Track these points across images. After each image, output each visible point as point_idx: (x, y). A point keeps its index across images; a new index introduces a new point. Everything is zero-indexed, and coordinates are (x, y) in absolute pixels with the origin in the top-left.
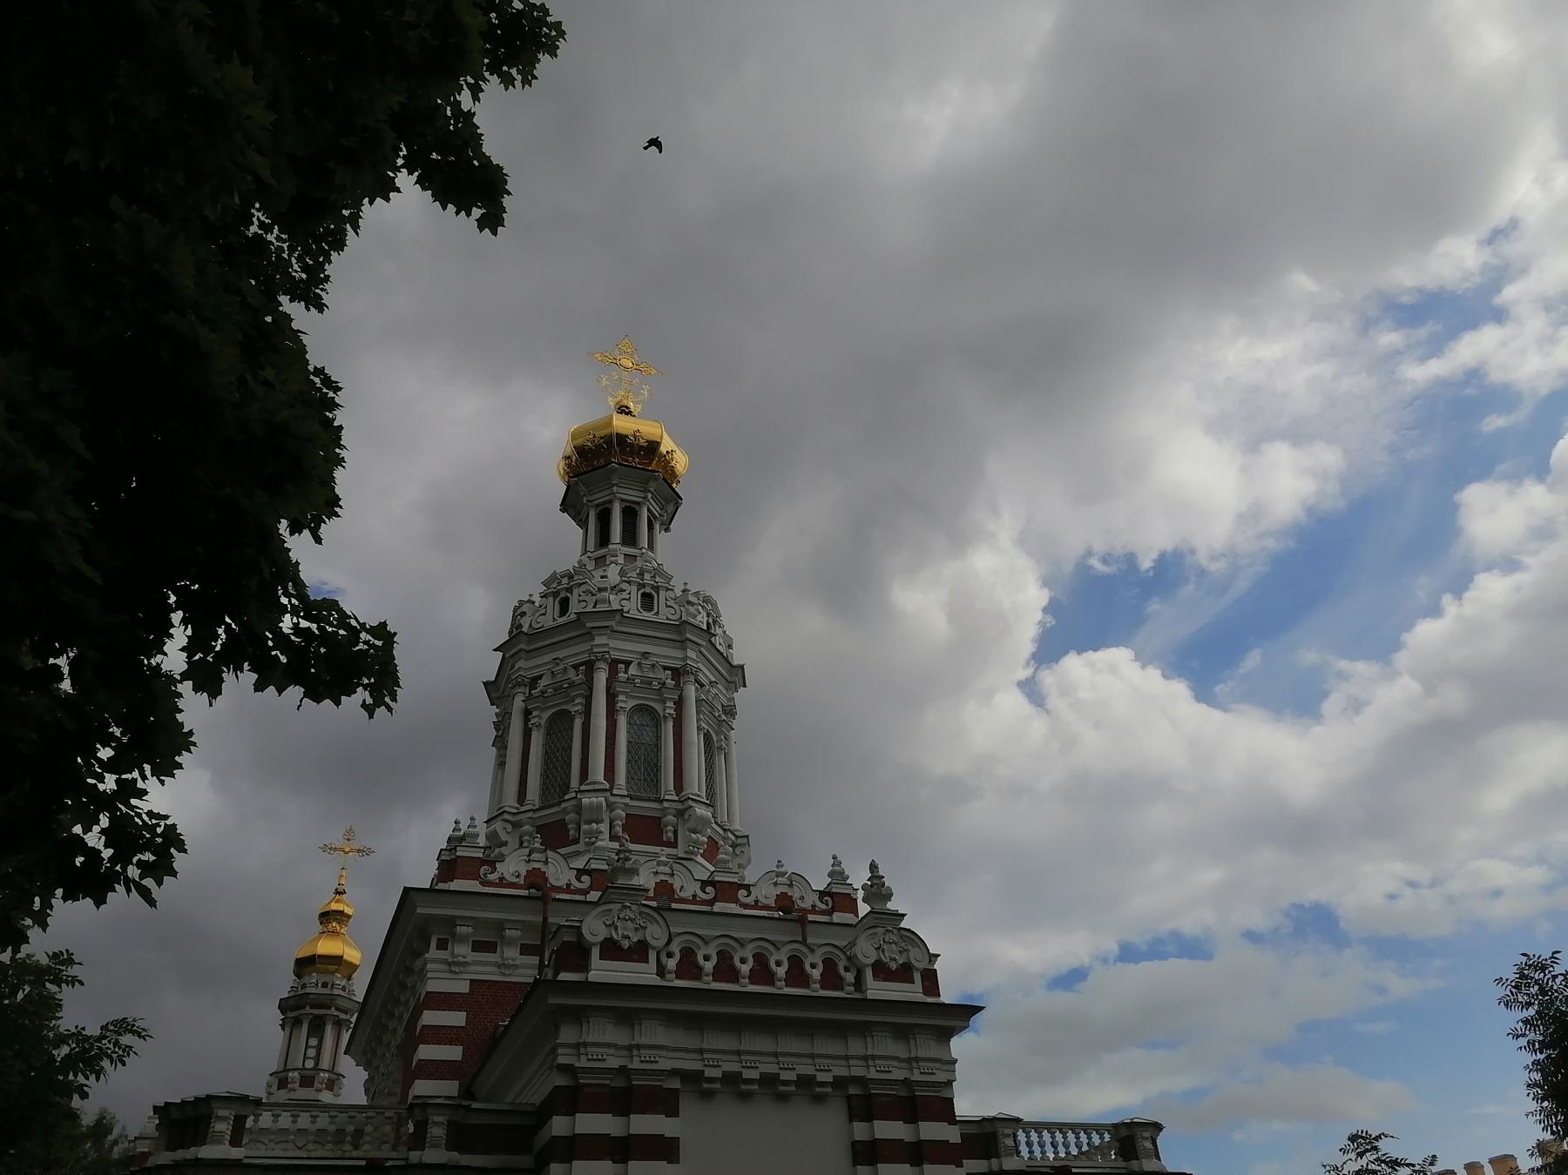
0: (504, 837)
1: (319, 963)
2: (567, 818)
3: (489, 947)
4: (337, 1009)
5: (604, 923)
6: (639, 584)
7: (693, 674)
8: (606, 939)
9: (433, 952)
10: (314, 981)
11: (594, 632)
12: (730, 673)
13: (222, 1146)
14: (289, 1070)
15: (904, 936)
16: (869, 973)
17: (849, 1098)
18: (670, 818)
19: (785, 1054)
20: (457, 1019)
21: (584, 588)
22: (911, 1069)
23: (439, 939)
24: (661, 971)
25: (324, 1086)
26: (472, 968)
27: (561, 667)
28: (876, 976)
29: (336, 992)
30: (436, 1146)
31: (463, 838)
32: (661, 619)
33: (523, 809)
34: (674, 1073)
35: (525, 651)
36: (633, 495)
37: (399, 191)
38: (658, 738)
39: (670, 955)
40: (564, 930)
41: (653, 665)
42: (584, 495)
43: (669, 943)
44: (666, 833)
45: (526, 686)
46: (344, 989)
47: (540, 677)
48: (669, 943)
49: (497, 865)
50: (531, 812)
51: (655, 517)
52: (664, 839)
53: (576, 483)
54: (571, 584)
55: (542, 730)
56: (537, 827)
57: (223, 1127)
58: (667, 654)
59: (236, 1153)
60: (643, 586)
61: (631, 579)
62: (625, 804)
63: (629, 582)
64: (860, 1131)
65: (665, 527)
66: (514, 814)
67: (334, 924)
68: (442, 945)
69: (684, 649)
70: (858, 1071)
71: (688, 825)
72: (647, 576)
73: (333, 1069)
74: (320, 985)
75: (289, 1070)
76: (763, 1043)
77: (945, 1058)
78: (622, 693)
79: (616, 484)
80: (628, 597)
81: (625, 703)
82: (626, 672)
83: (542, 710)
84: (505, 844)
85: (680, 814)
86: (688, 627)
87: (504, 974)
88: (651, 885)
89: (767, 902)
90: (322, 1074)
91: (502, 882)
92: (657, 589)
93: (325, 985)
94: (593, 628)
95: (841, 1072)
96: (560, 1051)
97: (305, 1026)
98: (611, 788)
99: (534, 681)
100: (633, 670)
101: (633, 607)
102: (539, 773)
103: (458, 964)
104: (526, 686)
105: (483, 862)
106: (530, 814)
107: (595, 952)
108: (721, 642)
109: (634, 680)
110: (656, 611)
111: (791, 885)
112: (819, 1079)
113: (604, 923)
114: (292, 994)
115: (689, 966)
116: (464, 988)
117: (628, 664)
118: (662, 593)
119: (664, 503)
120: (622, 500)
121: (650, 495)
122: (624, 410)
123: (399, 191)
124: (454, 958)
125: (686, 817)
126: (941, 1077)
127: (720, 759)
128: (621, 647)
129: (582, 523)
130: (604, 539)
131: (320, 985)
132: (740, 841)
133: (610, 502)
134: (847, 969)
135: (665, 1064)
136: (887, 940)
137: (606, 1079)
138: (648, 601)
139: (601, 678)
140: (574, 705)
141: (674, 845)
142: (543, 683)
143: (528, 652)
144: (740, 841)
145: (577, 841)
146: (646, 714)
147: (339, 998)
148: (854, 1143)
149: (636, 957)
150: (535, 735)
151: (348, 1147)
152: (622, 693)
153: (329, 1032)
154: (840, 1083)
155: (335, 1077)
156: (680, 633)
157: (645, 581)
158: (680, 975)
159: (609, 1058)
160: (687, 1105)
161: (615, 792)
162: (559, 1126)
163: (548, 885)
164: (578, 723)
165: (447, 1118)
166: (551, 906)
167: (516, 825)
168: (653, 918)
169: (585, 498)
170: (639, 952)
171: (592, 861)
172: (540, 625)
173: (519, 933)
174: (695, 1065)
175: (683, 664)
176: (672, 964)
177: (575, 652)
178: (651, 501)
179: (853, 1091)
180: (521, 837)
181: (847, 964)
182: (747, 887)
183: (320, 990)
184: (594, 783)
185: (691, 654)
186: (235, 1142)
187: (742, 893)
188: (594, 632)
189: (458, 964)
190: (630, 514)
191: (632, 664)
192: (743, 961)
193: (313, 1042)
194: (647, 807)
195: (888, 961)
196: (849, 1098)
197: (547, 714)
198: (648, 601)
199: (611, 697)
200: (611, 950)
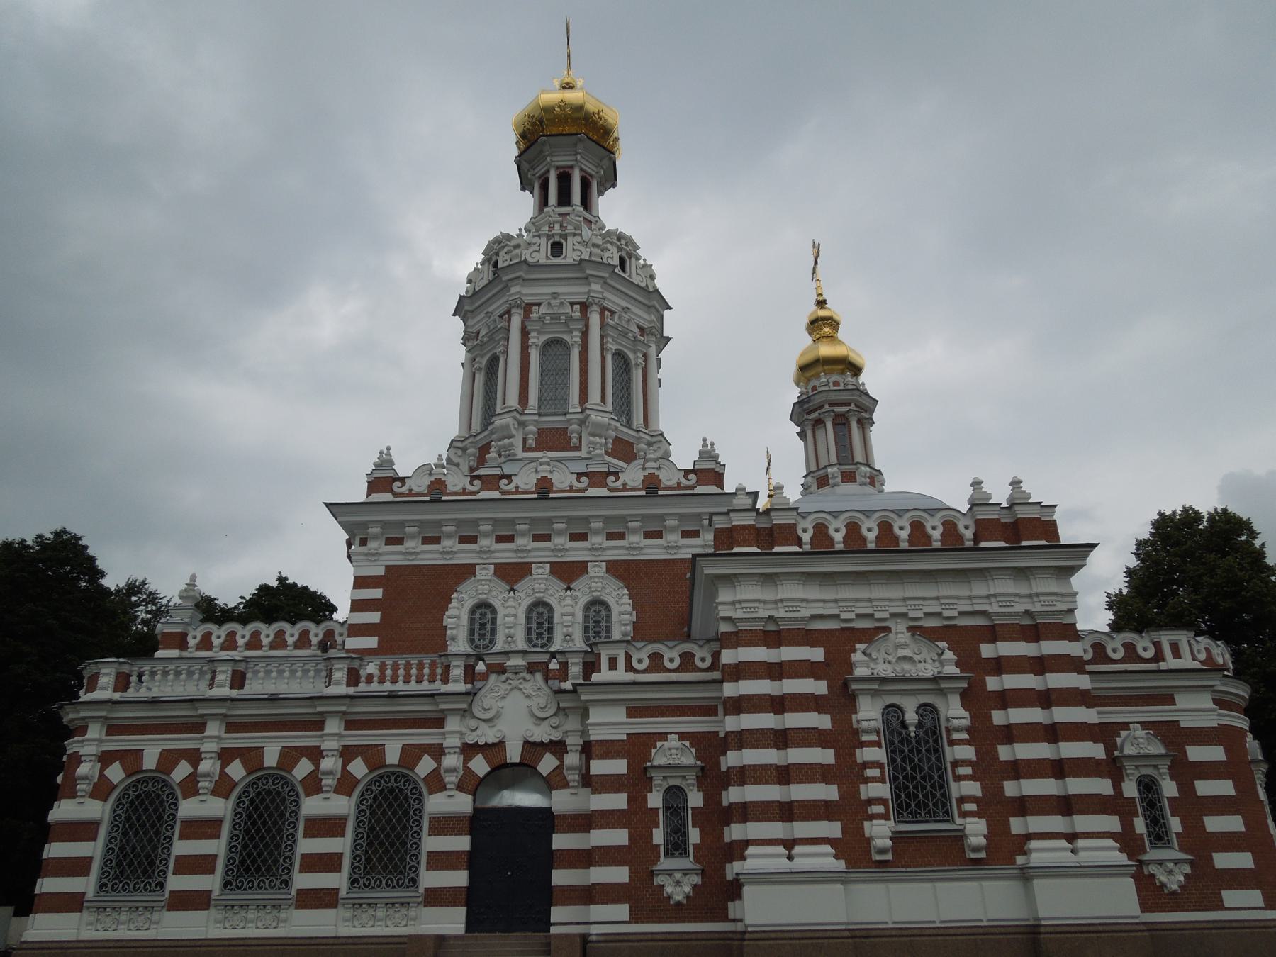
6: (548, 235)
7: (596, 304)
11: (591, 279)
12: (649, 299)
18: (643, 446)
19: (1001, 595)
22: (1033, 603)
26: (532, 554)
30: (456, 681)
32: (569, 261)
35: (469, 311)
36: (563, 161)
42: (529, 170)
49: (513, 478)
55: (483, 372)
58: (576, 292)
60: (553, 236)
66: (462, 441)
76: (894, 592)
77: (1070, 591)
78: (534, 330)
79: (580, 153)
80: (537, 249)
81: (536, 339)
85: (582, 423)
88: (639, 483)
89: (527, 487)
91: (410, 494)
94: (509, 280)
101: (542, 256)
102: (480, 407)
103: (560, 550)
105: (609, 474)
108: (639, 271)
112: (876, 617)
116: (380, 571)
118: (570, 239)
121: (579, 157)
122: (567, 86)
126: (1062, 607)
128: (529, 293)
130: (544, 202)
132: (655, 439)
137: (1016, 619)
139: (595, 319)
141: (579, 448)
143: (472, 312)
144: (655, 439)
146: (555, 347)
151: (438, 682)
152: (534, 330)
156: (583, 271)
159: (1016, 604)
173: (527, 526)
178: (583, 161)
182: (402, 480)
185: (596, 287)
187: (398, 484)
188: (591, 279)
190: (564, 179)
199: (525, 333)
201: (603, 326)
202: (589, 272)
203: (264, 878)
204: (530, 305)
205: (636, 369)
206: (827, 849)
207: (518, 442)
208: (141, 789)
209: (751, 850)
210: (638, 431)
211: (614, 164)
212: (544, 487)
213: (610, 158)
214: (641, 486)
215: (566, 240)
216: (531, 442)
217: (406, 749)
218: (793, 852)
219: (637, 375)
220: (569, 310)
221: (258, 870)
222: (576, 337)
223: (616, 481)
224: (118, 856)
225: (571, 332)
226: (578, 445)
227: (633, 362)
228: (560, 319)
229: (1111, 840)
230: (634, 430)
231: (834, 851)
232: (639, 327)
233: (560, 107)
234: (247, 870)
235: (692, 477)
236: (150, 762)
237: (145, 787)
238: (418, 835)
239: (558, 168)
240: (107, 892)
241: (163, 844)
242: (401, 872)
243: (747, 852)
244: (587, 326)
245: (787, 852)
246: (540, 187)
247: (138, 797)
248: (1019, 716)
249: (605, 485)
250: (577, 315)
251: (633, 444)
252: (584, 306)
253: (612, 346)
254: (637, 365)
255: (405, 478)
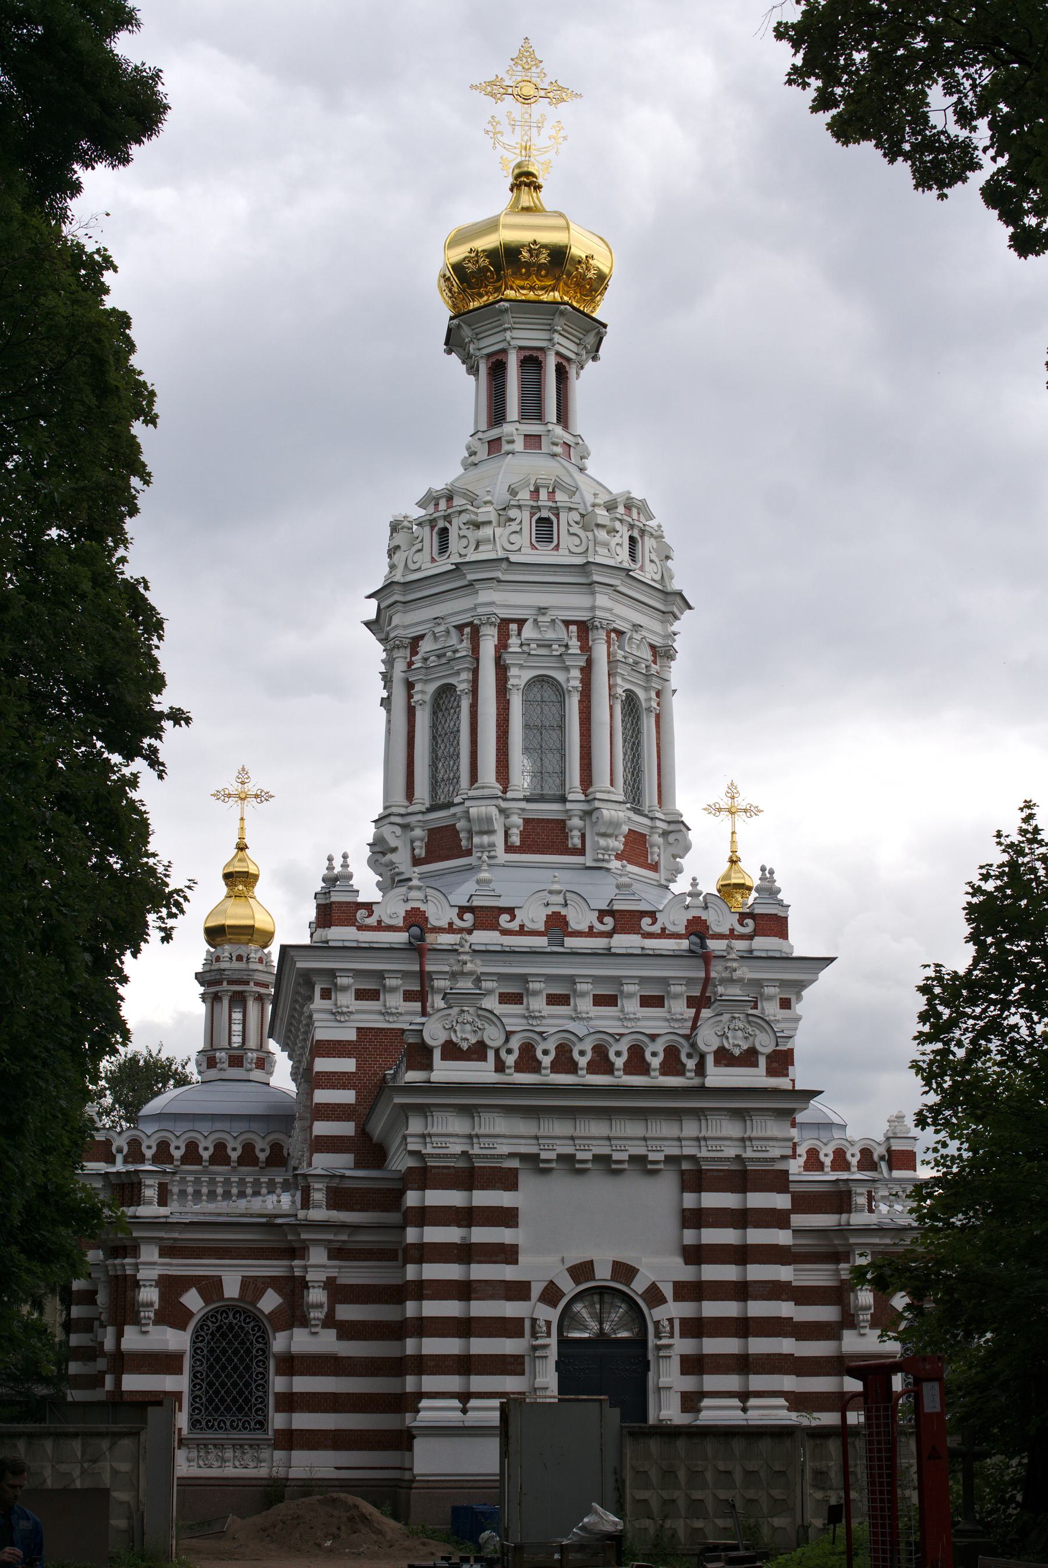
0: (393, 843)
1: (230, 934)
2: (459, 826)
3: (372, 995)
4: (257, 984)
5: (444, 1027)
6: (532, 507)
7: (603, 628)
8: (446, 1041)
9: (318, 1002)
10: (226, 954)
12: (665, 602)
13: (152, 1207)
14: (215, 1050)
15: (753, 1022)
16: (710, 1060)
17: (682, 1173)
20: (348, 1065)
21: (465, 517)
23: (322, 989)
24: (500, 1067)
25: (254, 1065)
27: (442, 628)
28: (717, 1062)
29: (252, 966)
31: (336, 879)
33: (411, 809)
34: (512, 1155)
37: (155, 427)
38: (563, 717)
39: (509, 1051)
40: (407, 1033)
41: (553, 621)
43: (507, 1040)
44: (572, 838)
45: (406, 647)
46: (261, 960)
47: (422, 637)
48: (507, 1040)
50: (420, 815)
51: (569, 360)
52: (570, 846)
53: (459, 326)
54: (449, 511)
56: (428, 830)
57: (150, 1193)
59: (163, 1211)
60: (539, 508)
61: (521, 502)
62: (523, 810)
63: (519, 507)
64: (689, 1200)
65: (593, 355)
66: (402, 815)
67: (241, 887)
68: (326, 994)
69: (593, 593)
70: (687, 1151)
71: (597, 829)
72: (543, 494)
73: (261, 1047)
74: (234, 958)
75: (215, 1050)
80: (518, 528)
81: (519, 677)
82: (519, 634)
83: (426, 681)
84: (394, 850)
86: (593, 567)
87: (389, 1022)
90: (249, 1054)
92: (556, 511)
93: (240, 958)
95: (676, 1151)
96: (409, 1140)
97: (226, 1003)
98: (505, 792)
99: (415, 642)
100: (528, 632)
103: (342, 1013)
104: (406, 647)
105: (644, 914)
106: (420, 817)
107: (437, 1054)
109: (529, 645)
110: (555, 542)
111: (706, 908)
113: (444, 1027)
114: (208, 968)
115: (528, 1061)
116: (351, 1035)
117: (521, 622)
118: (563, 516)
119: (581, 336)
120: (558, 354)
123: (155, 427)
124: (337, 1008)
125: (594, 819)
127: (648, 723)
129: (473, 370)
130: (497, 414)
131: (234, 958)
132: (672, 827)
133: (504, 351)
134: (689, 1056)
135: (504, 1149)
136: (732, 1027)
137: (451, 1162)
138: (545, 529)
139: (600, 652)
140: (460, 682)
141: (581, 852)
142: (425, 646)
144: (672, 827)
145: (469, 853)
147: (256, 973)
148: (684, 1210)
149: (475, 1056)
150: (419, 714)
153: (252, 1007)
154: (670, 1159)
155: (265, 1055)
156: (588, 574)
157: (540, 503)
158: (519, 1067)
160: (525, 1180)
161: (509, 795)
162: (412, 1198)
163: (429, 926)
164: (465, 704)
165: (325, 1185)
166: (429, 956)
167: (405, 827)
168: (491, 1020)
169: (472, 346)
170: (478, 1051)
171: (474, 898)
172: (416, 566)
174: (533, 1150)
175: (591, 614)
176: (510, 1060)
177: (456, 609)
179: (685, 1166)
180: (412, 842)
181: (691, 1051)
183: (236, 965)
184: (483, 788)
186: (163, 1202)
189: (342, 1013)
190: (532, 362)
191: (527, 624)
192: (582, 1053)
193: (237, 1016)
194: (549, 810)
195: (731, 1047)
196: (682, 1173)
197: (432, 688)
198: (545, 529)
200: (452, 1051)
201: (612, 662)
202: (596, 578)
203: (247, 1419)
204: (505, 622)
205: (648, 716)
206: (782, 1402)
207: (499, 839)
208: (221, 1320)
209: (424, 1403)
210: (652, 819)
211: (601, 339)
212: (557, 924)
213: (599, 333)
214: (543, 929)
215: (557, 516)
216: (516, 840)
217: (247, 1283)
218: (469, 1405)
219: (648, 724)
220: (454, 640)
221: (228, 1409)
222: (573, 680)
223: (653, 923)
224: (207, 1392)
225: (567, 669)
226: (580, 846)
227: (644, 705)
228: (538, 646)
229: (737, 1400)
230: (646, 816)
231: (787, 1404)
232: (652, 647)
233: (530, 251)
234: (217, 1409)
235: (609, 920)
236: (232, 1289)
237: (226, 1318)
238: (264, 1364)
239: (521, 348)
240: (201, 1429)
241: (256, 1381)
242: (246, 1415)
243: (420, 1405)
244: (589, 662)
245: (741, 1404)
246: (489, 374)
247: (219, 1328)
248: (434, 1234)
249: (494, 926)
250: (575, 644)
251: (646, 835)
252: (584, 629)
253: (621, 687)
254: (649, 710)
255: (371, 904)
